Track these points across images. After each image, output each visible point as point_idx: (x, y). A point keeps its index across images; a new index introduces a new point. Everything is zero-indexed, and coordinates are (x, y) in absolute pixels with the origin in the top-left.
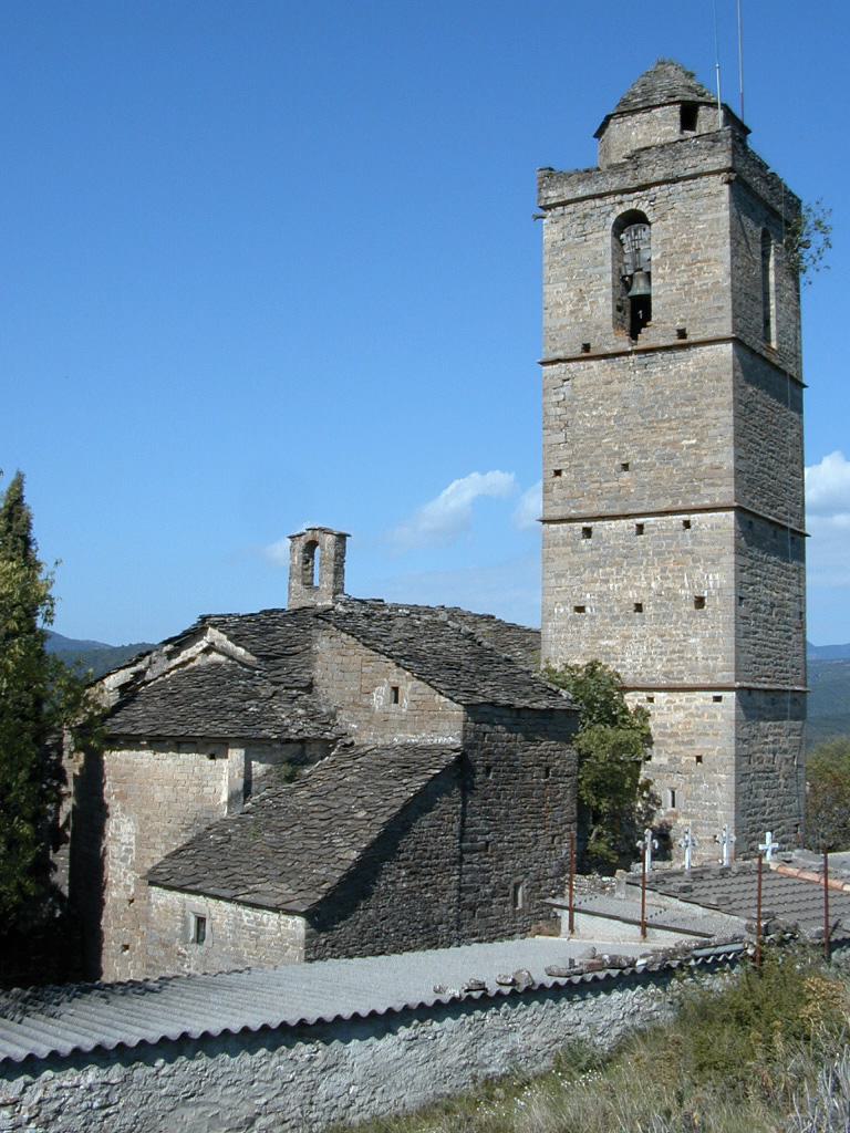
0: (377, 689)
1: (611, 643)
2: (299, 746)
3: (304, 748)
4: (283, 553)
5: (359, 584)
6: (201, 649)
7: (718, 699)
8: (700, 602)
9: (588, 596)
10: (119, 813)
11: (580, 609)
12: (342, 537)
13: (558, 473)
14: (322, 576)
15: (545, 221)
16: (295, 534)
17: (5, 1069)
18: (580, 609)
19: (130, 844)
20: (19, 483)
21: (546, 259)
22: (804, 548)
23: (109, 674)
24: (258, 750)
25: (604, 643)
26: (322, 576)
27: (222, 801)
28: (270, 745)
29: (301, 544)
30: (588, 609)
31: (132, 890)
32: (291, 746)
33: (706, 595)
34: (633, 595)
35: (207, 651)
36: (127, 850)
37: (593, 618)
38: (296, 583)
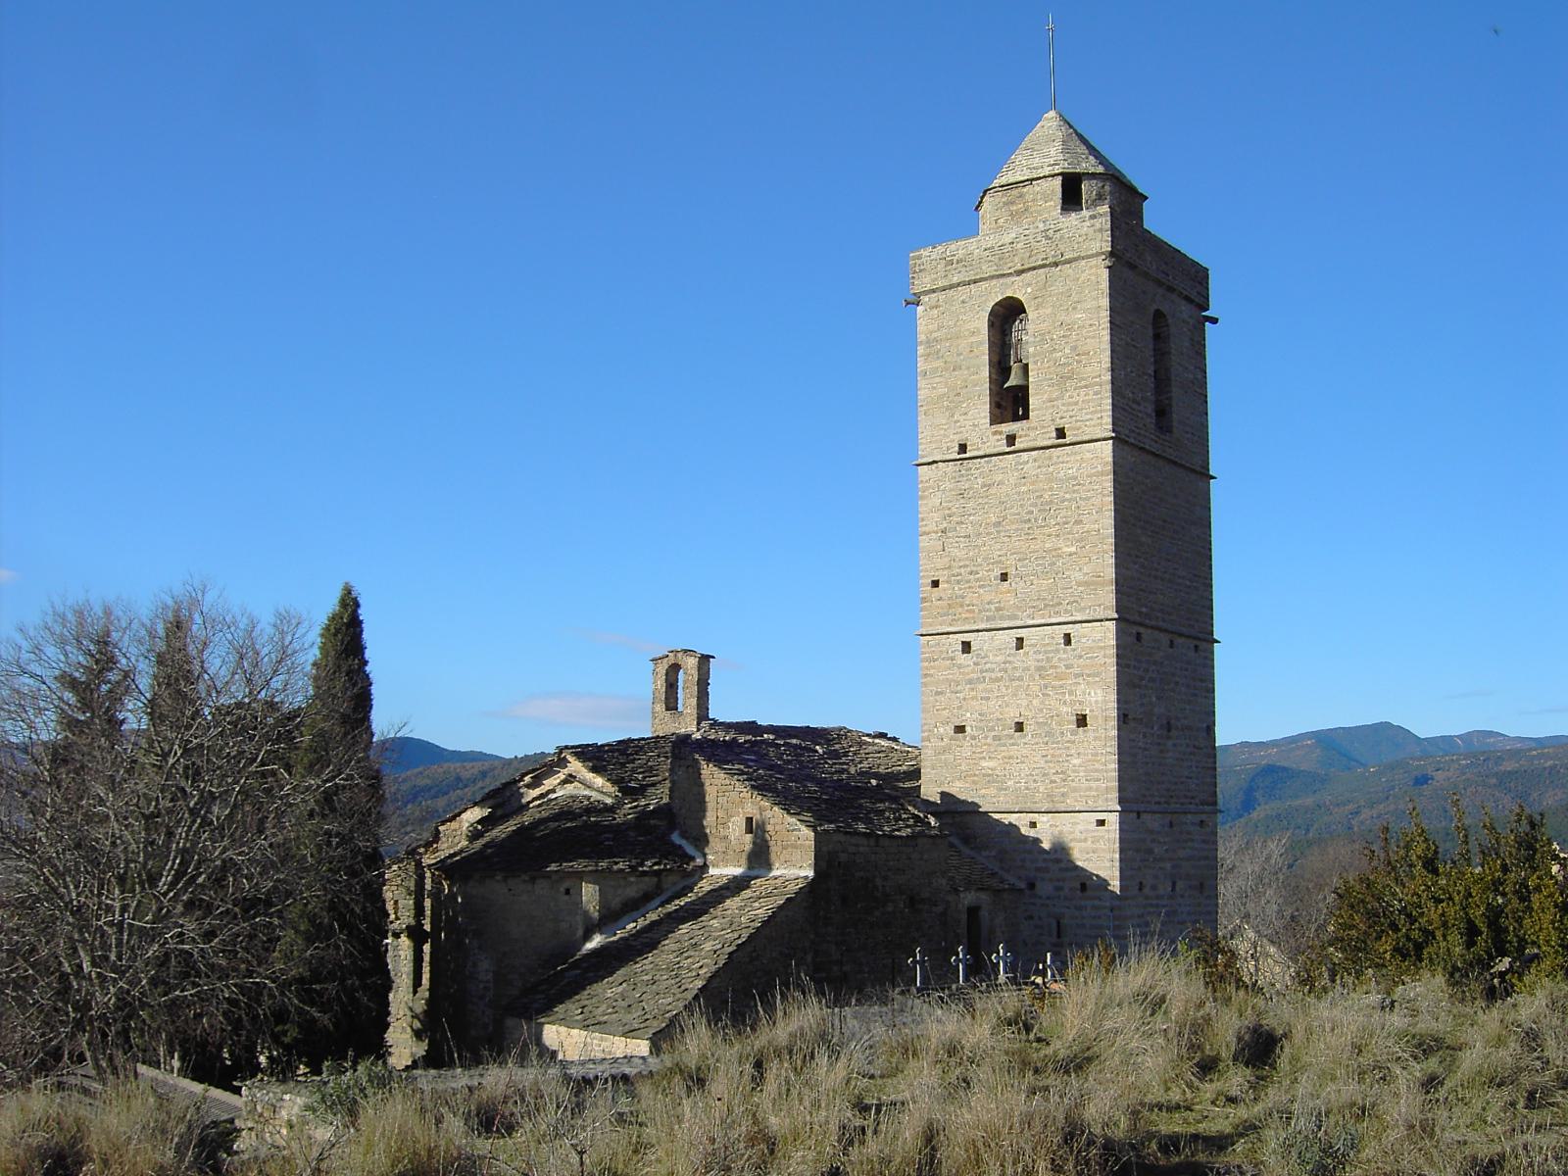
0: (732, 820)
1: (991, 764)
2: (655, 879)
3: (659, 881)
4: (650, 684)
5: (724, 709)
6: (558, 781)
7: (1101, 823)
8: (1082, 721)
9: (968, 715)
10: (476, 951)
11: (960, 729)
12: (705, 660)
13: (935, 584)
14: (687, 701)
15: (920, 309)
16: (658, 656)
17: (444, 1175)
18: (960, 729)
19: (488, 981)
20: (350, 604)
21: (921, 350)
22: (1208, 586)
23: (465, 810)
24: (612, 883)
25: (984, 764)
26: (687, 701)
27: (578, 936)
28: (625, 878)
29: (663, 668)
30: (968, 729)
31: (491, 1028)
32: (646, 879)
33: (1087, 712)
34: (1012, 715)
35: (565, 782)
36: (485, 988)
37: (973, 738)
38: (660, 707)
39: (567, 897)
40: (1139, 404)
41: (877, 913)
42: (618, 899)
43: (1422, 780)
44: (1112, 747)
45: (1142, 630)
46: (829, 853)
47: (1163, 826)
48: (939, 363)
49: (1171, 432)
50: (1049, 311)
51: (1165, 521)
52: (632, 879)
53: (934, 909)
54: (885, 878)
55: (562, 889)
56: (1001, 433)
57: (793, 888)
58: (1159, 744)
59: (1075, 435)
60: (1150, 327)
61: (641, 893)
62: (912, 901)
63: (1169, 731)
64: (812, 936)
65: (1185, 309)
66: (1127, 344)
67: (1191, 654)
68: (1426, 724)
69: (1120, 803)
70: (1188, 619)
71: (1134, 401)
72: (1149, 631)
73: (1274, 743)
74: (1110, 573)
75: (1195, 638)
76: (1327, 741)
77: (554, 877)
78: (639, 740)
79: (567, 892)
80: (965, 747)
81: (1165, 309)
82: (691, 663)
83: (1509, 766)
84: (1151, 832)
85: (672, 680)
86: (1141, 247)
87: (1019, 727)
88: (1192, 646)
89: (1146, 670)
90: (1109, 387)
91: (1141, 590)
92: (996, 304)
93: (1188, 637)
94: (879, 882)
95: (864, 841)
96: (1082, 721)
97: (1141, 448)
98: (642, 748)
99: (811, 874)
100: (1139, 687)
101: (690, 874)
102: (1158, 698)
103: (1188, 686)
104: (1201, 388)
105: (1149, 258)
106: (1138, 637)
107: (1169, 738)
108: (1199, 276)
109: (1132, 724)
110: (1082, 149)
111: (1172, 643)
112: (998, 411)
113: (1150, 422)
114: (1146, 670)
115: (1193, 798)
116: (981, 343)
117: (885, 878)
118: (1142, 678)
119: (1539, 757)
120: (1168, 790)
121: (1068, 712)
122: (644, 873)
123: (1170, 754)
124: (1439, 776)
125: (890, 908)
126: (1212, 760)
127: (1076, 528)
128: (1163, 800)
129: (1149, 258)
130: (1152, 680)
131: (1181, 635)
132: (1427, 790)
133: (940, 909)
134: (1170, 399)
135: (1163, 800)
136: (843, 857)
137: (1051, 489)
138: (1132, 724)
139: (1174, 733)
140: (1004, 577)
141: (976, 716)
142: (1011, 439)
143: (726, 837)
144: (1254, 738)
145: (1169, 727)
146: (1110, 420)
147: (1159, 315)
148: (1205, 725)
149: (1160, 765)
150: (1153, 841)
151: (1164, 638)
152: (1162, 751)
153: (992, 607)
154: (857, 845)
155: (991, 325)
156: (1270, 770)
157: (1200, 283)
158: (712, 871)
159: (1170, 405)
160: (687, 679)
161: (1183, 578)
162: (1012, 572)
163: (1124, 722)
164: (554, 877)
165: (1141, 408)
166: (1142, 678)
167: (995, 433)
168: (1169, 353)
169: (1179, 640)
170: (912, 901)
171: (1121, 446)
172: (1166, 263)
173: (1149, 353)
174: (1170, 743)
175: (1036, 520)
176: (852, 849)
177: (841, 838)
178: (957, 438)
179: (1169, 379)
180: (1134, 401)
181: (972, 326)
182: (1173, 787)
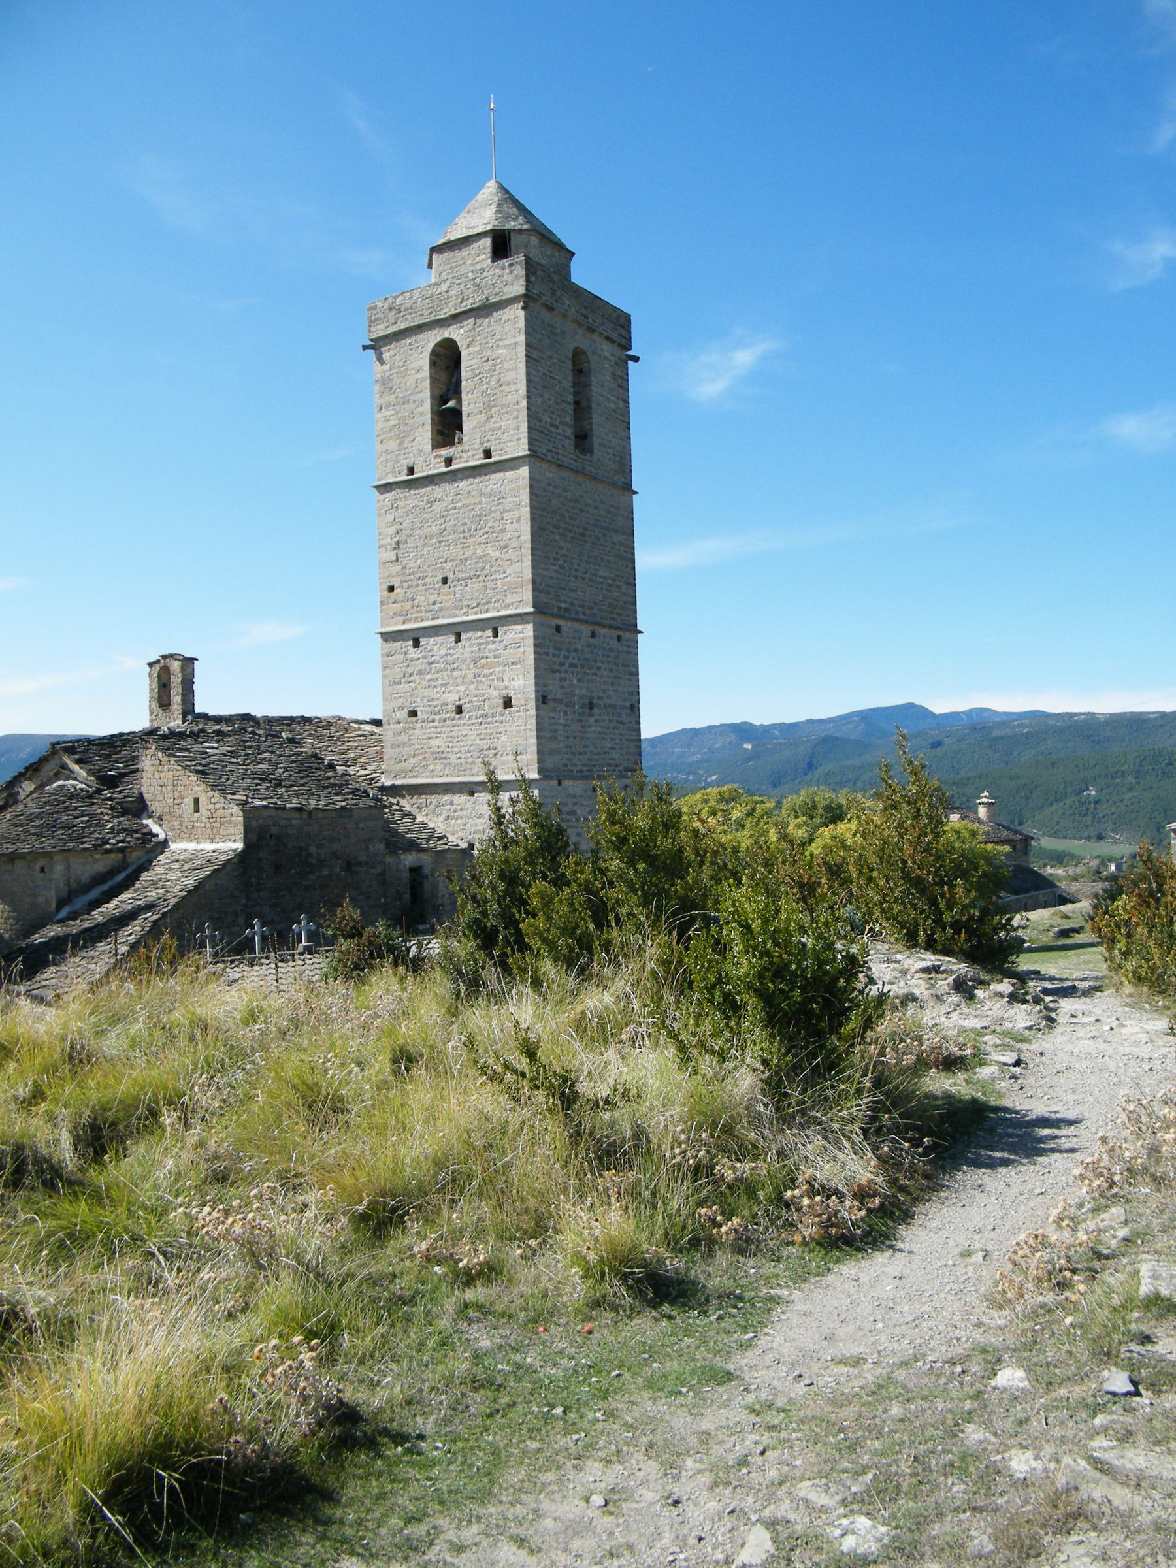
2: (120, 856)
3: (125, 857)
4: (142, 688)
8: (508, 703)
11: (413, 713)
12: (188, 662)
30: (419, 713)
32: (112, 855)
34: (452, 698)
39: (41, 875)
40: (557, 428)
41: (311, 877)
42: (87, 875)
43: (937, 744)
44: (532, 724)
45: (561, 622)
46: (260, 827)
47: (586, 791)
48: (392, 398)
49: (591, 453)
50: (477, 349)
51: (585, 529)
52: (98, 856)
53: (373, 871)
54: (319, 846)
55: (37, 867)
56: (440, 456)
57: (222, 858)
58: (580, 721)
59: (500, 455)
60: (570, 362)
61: (108, 868)
62: (349, 865)
63: (591, 709)
64: (244, 901)
65: (606, 349)
66: (545, 375)
67: (614, 643)
68: (939, 706)
69: (539, 772)
70: (612, 613)
71: (552, 425)
72: (569, 624)
73: (830, 720)
74: (528, 574)
75: (618, 628)
76: (868, 717)
77: (29, 858)
78: (129, 734)
79: (42, 870)
80: (418, 730)
81: (585, 346)
82: (176, 666)
83: (997, 733)
84: (574, 796)
85: (164, 681)
86: (559, 293)
87: (459, 710)
88: (615, 636)
89: (566, 657)
90: (525, 413)
91: (561, 588)
92: (436, 345)
93: (611, 627)
94: (313, 850)
95: (297, 815)
96: (508, 703)
97: (559, 466)
98: (129, 740)
99: (240, 846)
100: (559, 672)
101: (152, 850)
102: (579, 681)
103: (611, 670)
104: (623, 415)
105: (567, 303)
106: (558, 629)
107: (591, 715)
108: (622, 322)
109: (552, 704)
110: (514, 211)
111: (593, 635)
112: (440, 438)
113: (570, 444)
114: (566, 657)
115: (616, 765)
116: (423, 380)
117: (319, 846)
118: (562, 664)
119: (1020, 725)
120: (590, 760)
121: (495, 696)
122: (108, 851)
123: (593, 729)
124: (947, 741)
125: (326, 872)
126: (542, 734)
127: (501, 536)
128: (585, 769)
129: (567, 303)
130: (572, 665)
131: (603, 626)
132: (939, 751)
133: (379, 870)
134: (591, 424)
135: (585, 769)
136: (274, 830)
137: (480, 503)
138: (552, 704)
139: (595, 711)
140: (445, 581)
141: (425, 702)
142: (449, 461)
143: (181, 816)
144: (816, 716)
145: (591, 706)
146: (526, 441)
147: (578, 356)
148: (628, 704)
149: (582, 738)
150: (575, 804)
151: (586, 629)
152: (583, 727)
153: (436, 607)
154: (290, 819)
155: (433, 364)
156: (826, 740)
157: (622, 327)
158: (173, 846)
159: (591, 430)
160: (176, 681)
161: (605, 578)
162: (451, 576)
163: (544, 702)
164: (29, 858)
165: (560, 431)
166: (562, 664)
167: (436, 457)
168: (589, 385)
169: (602, 631)
170: (349, 865)
171: (538, 463)
172: (586, 308)
173: (568, 384)
174: (592, 720)
175: (469, 530)
176: (282, 823)
177: (273, 813)
178: (405, 462)
179: (590, 408)
180: (552, 425)
181: (416, 365)
182: (596, 757)
